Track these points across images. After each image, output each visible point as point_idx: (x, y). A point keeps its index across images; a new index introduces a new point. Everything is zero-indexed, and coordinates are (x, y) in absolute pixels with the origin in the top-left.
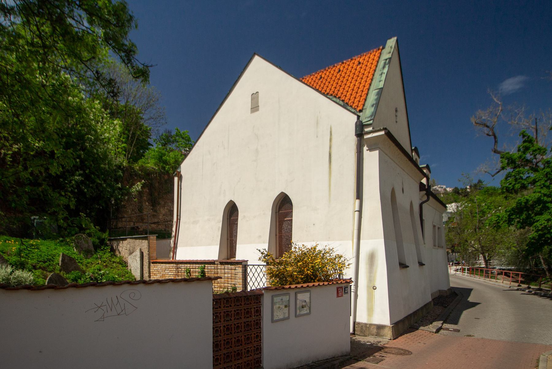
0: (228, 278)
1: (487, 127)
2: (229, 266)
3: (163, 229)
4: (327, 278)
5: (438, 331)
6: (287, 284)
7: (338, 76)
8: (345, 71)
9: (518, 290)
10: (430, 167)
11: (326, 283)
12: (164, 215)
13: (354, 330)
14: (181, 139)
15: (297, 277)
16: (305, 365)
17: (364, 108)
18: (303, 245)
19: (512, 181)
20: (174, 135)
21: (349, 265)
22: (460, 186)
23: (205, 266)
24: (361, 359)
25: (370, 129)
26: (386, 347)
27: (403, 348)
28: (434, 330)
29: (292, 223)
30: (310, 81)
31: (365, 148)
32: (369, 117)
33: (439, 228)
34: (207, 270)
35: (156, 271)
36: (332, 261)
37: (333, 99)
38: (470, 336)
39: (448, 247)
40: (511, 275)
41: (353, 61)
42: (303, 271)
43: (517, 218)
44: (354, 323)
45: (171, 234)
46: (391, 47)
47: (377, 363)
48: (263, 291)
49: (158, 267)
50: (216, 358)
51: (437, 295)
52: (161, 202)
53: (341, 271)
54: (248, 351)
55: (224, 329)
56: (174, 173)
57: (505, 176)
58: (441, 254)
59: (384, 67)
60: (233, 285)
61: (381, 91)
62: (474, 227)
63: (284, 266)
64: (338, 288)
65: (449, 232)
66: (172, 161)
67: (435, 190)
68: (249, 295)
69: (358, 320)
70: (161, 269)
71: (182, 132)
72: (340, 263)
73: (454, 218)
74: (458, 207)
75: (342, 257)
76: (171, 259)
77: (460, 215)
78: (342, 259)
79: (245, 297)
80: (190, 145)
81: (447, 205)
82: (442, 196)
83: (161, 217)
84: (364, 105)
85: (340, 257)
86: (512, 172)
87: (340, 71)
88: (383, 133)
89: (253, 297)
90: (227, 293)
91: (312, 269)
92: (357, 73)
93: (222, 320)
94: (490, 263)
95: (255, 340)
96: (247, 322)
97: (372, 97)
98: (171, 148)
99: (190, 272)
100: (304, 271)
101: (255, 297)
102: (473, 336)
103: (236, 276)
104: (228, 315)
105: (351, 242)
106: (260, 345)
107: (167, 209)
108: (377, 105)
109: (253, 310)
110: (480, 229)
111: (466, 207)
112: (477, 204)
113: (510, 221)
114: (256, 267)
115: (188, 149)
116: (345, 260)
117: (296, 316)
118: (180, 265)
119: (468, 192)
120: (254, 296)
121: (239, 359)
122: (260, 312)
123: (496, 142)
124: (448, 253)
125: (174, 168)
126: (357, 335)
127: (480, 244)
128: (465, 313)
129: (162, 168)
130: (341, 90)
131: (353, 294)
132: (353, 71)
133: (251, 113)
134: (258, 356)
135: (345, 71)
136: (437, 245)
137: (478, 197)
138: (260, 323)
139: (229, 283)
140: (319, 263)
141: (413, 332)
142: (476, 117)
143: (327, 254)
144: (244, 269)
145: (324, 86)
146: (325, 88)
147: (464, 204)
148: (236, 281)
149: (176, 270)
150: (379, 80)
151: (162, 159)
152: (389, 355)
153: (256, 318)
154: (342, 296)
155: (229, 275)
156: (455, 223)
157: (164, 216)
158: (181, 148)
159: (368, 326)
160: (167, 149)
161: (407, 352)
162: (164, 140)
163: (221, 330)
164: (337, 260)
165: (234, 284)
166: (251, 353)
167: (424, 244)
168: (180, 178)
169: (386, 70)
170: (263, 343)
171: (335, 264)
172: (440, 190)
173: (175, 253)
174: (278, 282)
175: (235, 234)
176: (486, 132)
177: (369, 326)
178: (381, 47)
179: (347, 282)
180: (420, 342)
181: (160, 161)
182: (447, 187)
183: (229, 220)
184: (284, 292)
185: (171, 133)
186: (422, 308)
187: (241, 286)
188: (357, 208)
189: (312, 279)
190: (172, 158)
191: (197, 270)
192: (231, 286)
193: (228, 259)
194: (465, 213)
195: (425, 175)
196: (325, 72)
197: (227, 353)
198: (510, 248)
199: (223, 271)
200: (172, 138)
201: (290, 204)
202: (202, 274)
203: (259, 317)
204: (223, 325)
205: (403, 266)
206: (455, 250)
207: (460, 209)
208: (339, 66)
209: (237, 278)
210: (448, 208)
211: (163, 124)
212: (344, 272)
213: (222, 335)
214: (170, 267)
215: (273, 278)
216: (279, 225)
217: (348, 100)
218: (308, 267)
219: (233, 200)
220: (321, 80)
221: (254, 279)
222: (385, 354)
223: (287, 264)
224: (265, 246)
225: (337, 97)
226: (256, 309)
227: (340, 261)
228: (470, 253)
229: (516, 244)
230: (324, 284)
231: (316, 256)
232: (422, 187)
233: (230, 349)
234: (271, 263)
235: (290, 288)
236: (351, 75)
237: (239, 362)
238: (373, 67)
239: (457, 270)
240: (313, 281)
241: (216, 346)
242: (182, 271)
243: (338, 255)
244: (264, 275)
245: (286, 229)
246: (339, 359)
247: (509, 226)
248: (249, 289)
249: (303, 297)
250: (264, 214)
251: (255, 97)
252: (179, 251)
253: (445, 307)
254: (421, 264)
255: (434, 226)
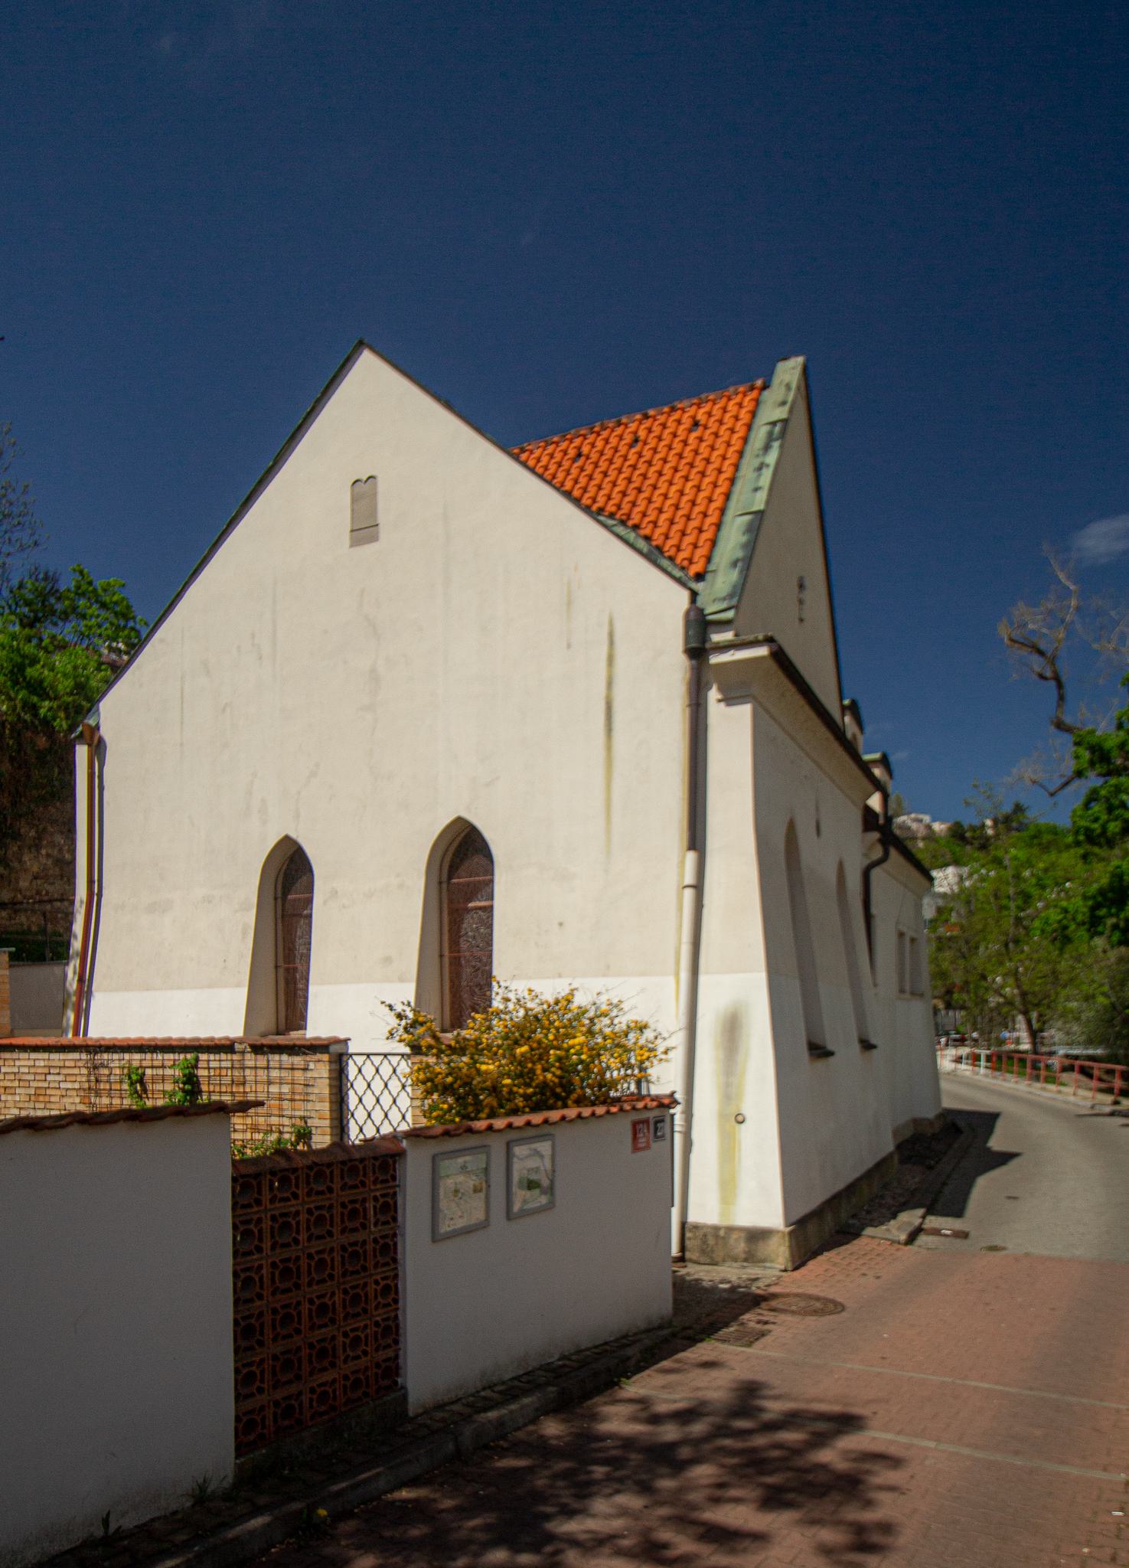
0: (281, 1099)
1: (1041, 653)
2: (285, 1057)
3: (34, 928)
4: (603, 1095)
5: (912, 1238)
6: (483, 1115)
7: (632, 458)
8: (652, 443)
9: (1112, 1114)
10: (892, 759)
11: (600, 1110)
12: (36, 878)
13: (683, 1248)
14: (94, 609)
15: (511, 1092)
16: (539, 1369)
17: (711, 567)
18: (530, 991)
19: (1099, 812)
20: (69, 590)
21: (666, 1052)
22: (968, 820)
23: (197, 1060)
24: (703, 1336)
25: (728, 636)
26: (774, 1296)
27: (822, 1294)
28: (903, 1237)
29: (492, 916)
30: (545, 460)
31: (714, 694)
32: (724, 599)
33: (913, 940)
34: (205, 1073)
35: (12, 1077)
36: (618, 1043)
37: (615, 529)
38: (994, 1248)
39: (936, 993)
40: (1096, 1072)
41: (676, 415)
42: (532, 1071)
43: (1112, 915)
44: (683, 1225)
45: (68, 945)
46: (788, 387)
47: (750, 1344)
48: (404, 1144)
49: (18, 1063)
50: (245, 1371)
51: (908, 1133)
52: (23, 831)
53: (642, 1069)
54: (357, 1339)
55: (273, 1274)
56: (72, 728)
57: (1082, 800)
58: (917, 1013)
59: (767, 448)
60: (298, 1122)
61: (758, 522)
62: (1003, 938)
63: (472, 1058)
64: (635, 1124)
65: (939, 949)
66: (64, 685)
67: (904, 827)
68: (357, 1156)
69: (693, 1218)
70: (32, 1070)
71: (99, 584)
72: (641, 1048)
73: (951, 910)
74: (961, 879)
75: (646, 1026)
76: (70, 1035)
77: (968, 902)
78: (649, 1034)
79: (343, 1163)
80: (133, 634)
81: (934, 873)
82: (921, 844)
83: (23, 884)
84: (709, 559)
85: (642, 1028)
86: (1101, 787)
87: (636, 441)
88: (763, 651)
89: (372, 1161)
90: (280, 1152)
91: (560, 1068)
92: (688, 453)
93: (267, 1245)
94: (1043, 1038)
95: (379, 1303)
96: (351, 1244)
97: (733, 538)
98: (60, 637)
99: (141, 1081)
100: (534, 1074)
101: (377, 1164)
102: (1004, 1249)
103: (310, 1090)
104: (286, 1226)
105: (672, 979)
106: (396, 1317)
107: (48, 855)
108: (746, 563)
109: (370, 1205)
110: (1017, 942)
111: (983, 879)
112: (1010, 872)
113: (1093, 924)
114: (377, 1060)
115: (121, 646)
116: (656, 1038)
117: (509, 1216)
118: (105, 1056)
119: (988, 839)
120: (375, 1158)
121: (325, 1369)
122: (396, 1211)
123: (1061, 698)
124: (936, 1011)
125: (72, 710)
126: (691, 1261)
127: (1019, 987)
128: (982, 1182)
129: (23, 708)
130: (642, 505)
131: (678, 1139)
132: (677, 446)
133: (352, 546)
134: (390, 1353)
135: (652, 443)
136: (907, 988)
137: (1014, 852)
138: (395, 1244)
139: (285, 1113)
140: (582, 1049)
141: (847, 1243)
142: (1011, 623)
143: (602, 1019)
144: (335, 1066)
145: (588, 484)
146: (592, 490)
147: (977, 872)
148: (310, 1106)
149: (89, 1074)
150: (753, 487)
151: (25, 678)
152: (782, 1317)
153: (380, 1231)
154: (648, 1147)
155: (286, 1089)
156: (955, 925)
157: (39, 882)
158: (96, 640)
159: (722, 1233)
160: (41, 640)
161: (831, 1306)
162: (28, 603)
163: (261, 1278)
164: (631, 1036)
165: (304, 1118)
166: (366, 1345)
167: (875, 985)
168: (98, 749)
169: (772, 458)
170: (404, 1311)
171: (627, 1050)
172: (914, 826)
173: (83, 1012)
174: (451, 1108)
175: (302, 950)
176: (1037, 669)
177: (726, 1233)
178: (759, 383)
179: (661, 1106)
180: (864, 1275)
181: (16, 683)
182: (934, 820)
183: (279, 901)
184: (472, 1141)
185: (55, 580)
186: (868, 1175)
187: (327, 1123)
188: (689, 878)
189: (557, 1097)
190: (65, 675)
191: (169, 1072)
192: (293, 1125)
193: (278, 1033)
194: (981, 898)
195: (878, 786)
196: (591, 438)
197: (283, 1353)
198: (1093, 996)
199: (262, 1075)
200: (59, 599)
201: (485, 856)
202: (188, 1087)
203: (392, 1225)
204: (270, 1261)
205: (819, 1051)
206: (953, 1003)
207: (967, 884)
208: (634, 425)
209: (311, 1097)
210: (936, 882)
211: (22, 549)
212: (653, 1072)
213: (265, 1293)
214: (67, 1064)
215: (435, 1096)
216: (450, 922)
217: (662, 537)
218: (547, 1061)
219: (293, 835)
220: (579, 463)
221: (369, 1101)
222: (772, 1313)
223: (476, 1049)
224: (405, 993)
225: (630, 523)
226: (381, 1200)
227: (642, 1042)
228: (992, 1010)
229: (1106, 988)
230: (593, 1114)
231: (570, 1025)
232: (870, 819)
233: (296, 1338)
234: (430, 1047)
235: (490, 1128)
236: (672, 459)
237: (324, 1380)
238: (736, 444)
239: (958, 1060)
240: (560, 1103)
241: (246, 1332)
242: (112, 1077)
243: (636, 1022)
244: (404, 1087)
245: (474, 938)
246: (639, 1340)
247: (1092, 937)
248: (354, 1135)
249: (531, 1158)
250: (401, 886)
251: (364, 490)
252: (99, 1003)
253: (931, 1168)
254: (867, 1046)
255: (901, 935)
